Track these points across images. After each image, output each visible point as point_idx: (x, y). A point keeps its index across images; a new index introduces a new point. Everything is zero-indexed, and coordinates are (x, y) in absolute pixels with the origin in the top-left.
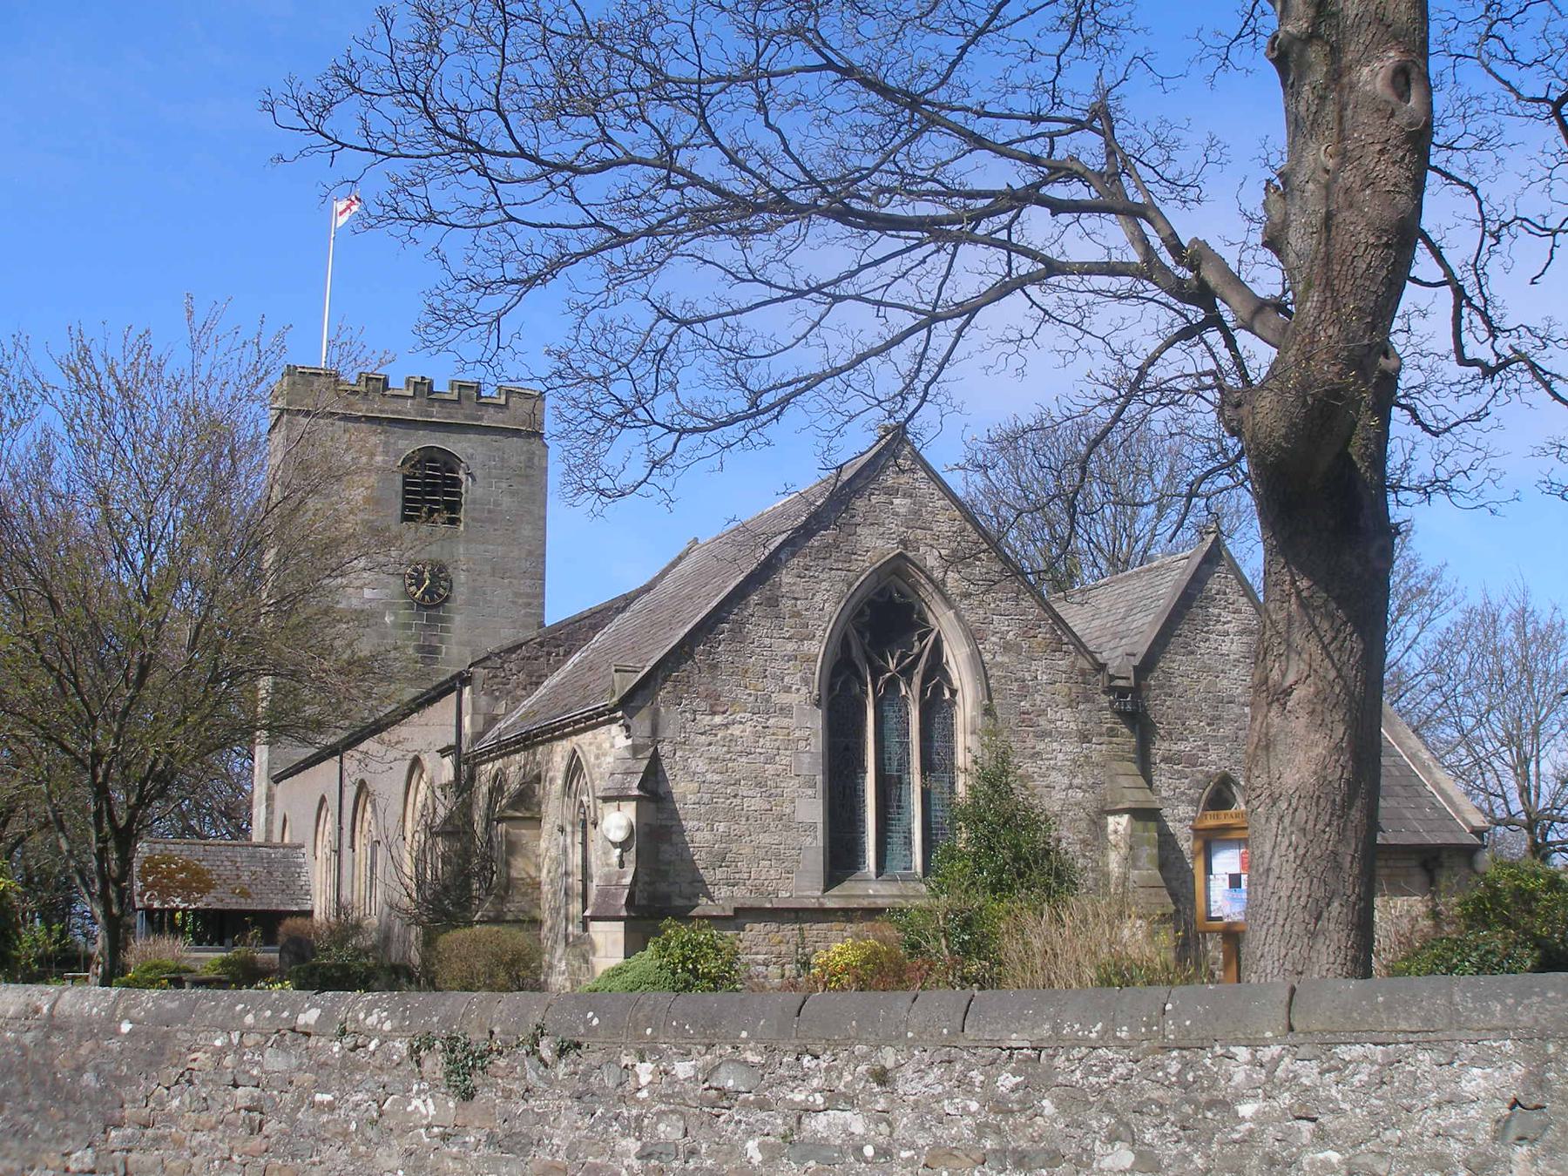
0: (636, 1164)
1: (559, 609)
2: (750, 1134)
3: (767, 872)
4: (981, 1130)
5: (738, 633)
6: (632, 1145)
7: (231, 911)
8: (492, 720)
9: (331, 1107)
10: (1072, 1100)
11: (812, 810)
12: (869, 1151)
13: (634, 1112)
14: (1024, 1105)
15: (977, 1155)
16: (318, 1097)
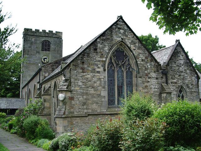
3: (94, 106)
5: (88, 56)
8: (45, 77)
11: (104, 93)
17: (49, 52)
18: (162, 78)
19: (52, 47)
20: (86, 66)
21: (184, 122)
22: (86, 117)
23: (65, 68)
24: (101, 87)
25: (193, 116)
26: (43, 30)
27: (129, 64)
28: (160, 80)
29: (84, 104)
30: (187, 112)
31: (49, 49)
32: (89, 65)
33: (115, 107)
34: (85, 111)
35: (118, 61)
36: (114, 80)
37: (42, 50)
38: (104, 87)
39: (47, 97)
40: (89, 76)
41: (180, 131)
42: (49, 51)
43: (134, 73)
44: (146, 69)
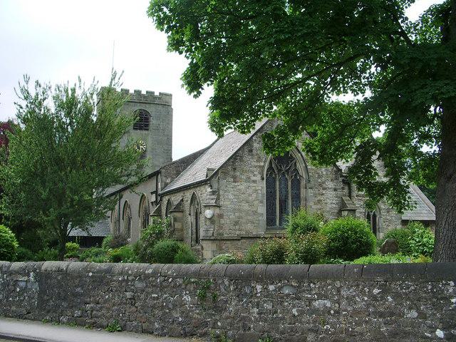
0: (257, 316)
1: (177, 155)
2: (294, 307)
3: (249, 227)
4: (368, 305)
5: (241, 160)
6: (256, 310)
7: (98, 237)
8: (166, 185)
9: (157, 298)
10: (397, 296)
11: (262, 209)
12: (332, 312)
13: (256, 300)
14: (382, 298)
15: (367, 313)
16: (153, 295)
17: (146, 132)
18: (343, 188)
19: (153, 122)
20: (238, 174)
21: (347, 238)
22: (239, 240)
23: (212, 176)
24: (258, 202)
25: (356, 233)
26: (135, 91)
27: (296, 170)
28: (339, 193)
29: (236, 223)
30: (351, 229)
31: (147, 126)
32: (243, 171)
33: (276, 229)
34: (238, 232)
35: (280, 166)
36: (275, 192)
37: (134, 129)
38: (261, 202)
39: (178, 215)
40: (242, 187)
41: (342, 246)
42: (147, 130)
43: (303, 183)
44: (320, 177)
